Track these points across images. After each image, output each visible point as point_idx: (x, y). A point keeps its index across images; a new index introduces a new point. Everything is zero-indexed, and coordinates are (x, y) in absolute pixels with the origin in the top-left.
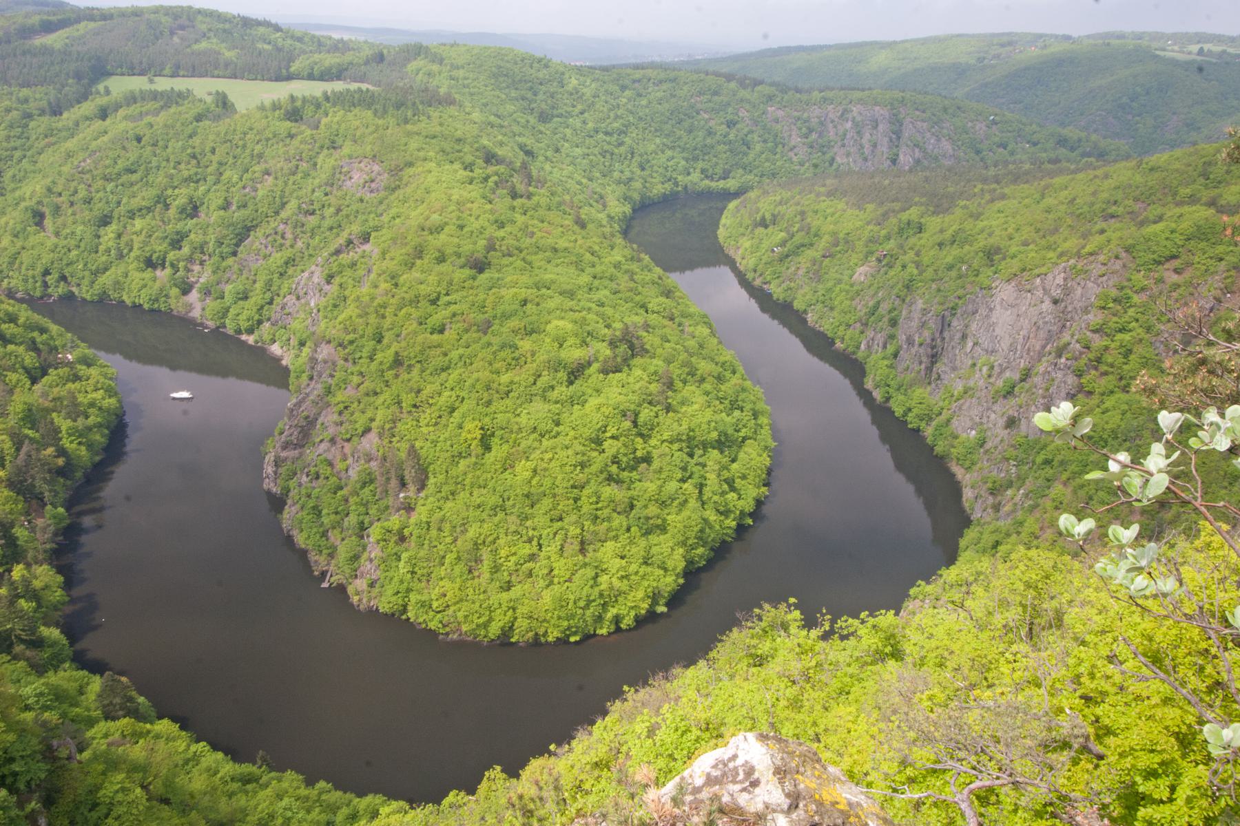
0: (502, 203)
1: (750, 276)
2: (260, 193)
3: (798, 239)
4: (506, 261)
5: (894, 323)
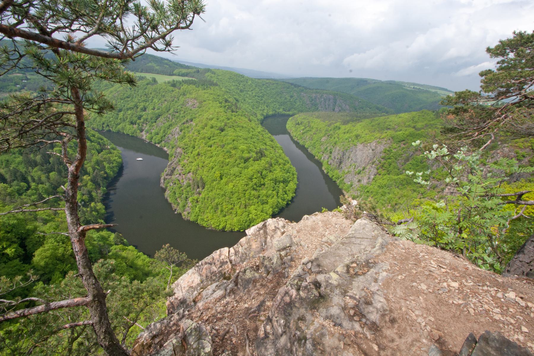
0: (229, 113)
1: (294, 138)
2: (163, 106)
3: (307, 129)
4: (229, 129)
5: (331, 153)
